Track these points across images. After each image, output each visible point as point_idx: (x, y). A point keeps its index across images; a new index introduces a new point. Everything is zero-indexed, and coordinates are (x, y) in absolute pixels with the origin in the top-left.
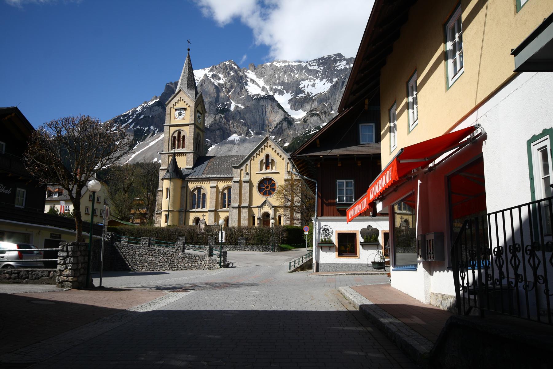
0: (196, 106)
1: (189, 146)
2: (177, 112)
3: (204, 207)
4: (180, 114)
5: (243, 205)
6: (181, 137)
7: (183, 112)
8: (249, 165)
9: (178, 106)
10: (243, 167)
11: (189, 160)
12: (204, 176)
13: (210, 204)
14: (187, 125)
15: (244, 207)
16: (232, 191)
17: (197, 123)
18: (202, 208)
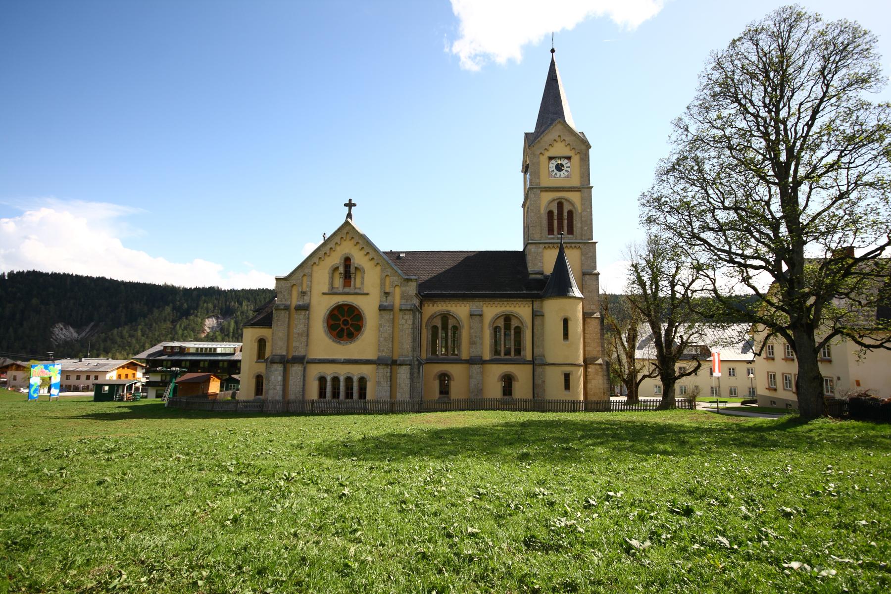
2: (554, 163)
4: (559, 168)
6: (565, 214)
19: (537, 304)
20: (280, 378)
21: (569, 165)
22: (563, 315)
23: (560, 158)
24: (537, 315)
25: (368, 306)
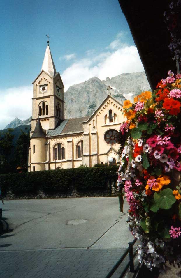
0: (55, 83)
1: (51, 112)
2: (41, 88)
3: (63, 158)
5: (92, 153)
6: (45, 107)
7: (46, 87)
8: (95, 120)
9: (41, 84)
10: (91, 122)
11: (51, 123)
12: (63, 134)
13: (68, 156)
14: (49, 97)
15: (93, 155)
16: (84, 143)
17: (57, 95)
18: (63, 159)
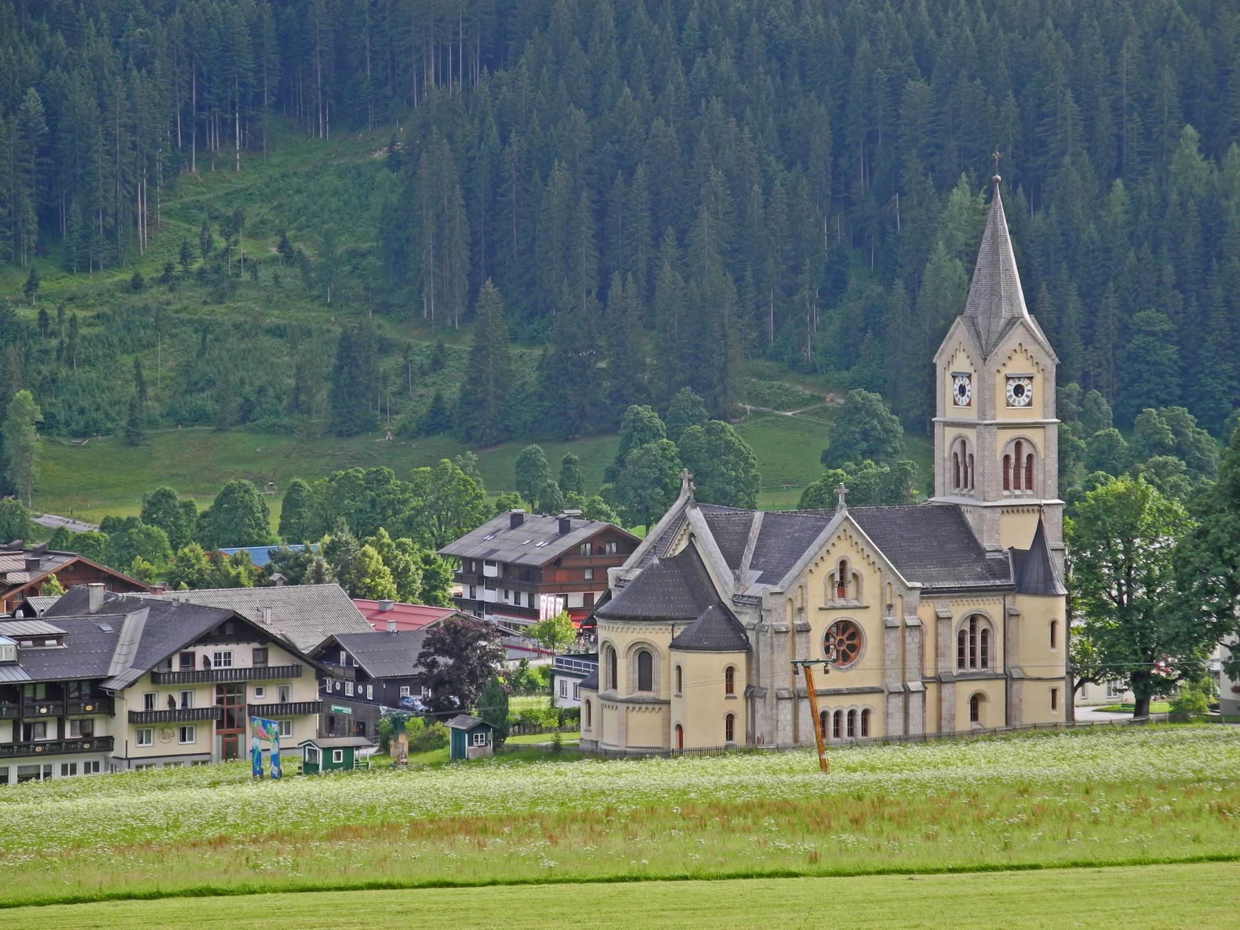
2: (1013, 384)
6: (1024, 460)
9: (1008, 371)
19: (1009, 599)
20: (789, 717)
21: (1029, 387)
22: (1050, 618)
23: (1019, 378)
24: (1009, 615)
25: (868, 623)
